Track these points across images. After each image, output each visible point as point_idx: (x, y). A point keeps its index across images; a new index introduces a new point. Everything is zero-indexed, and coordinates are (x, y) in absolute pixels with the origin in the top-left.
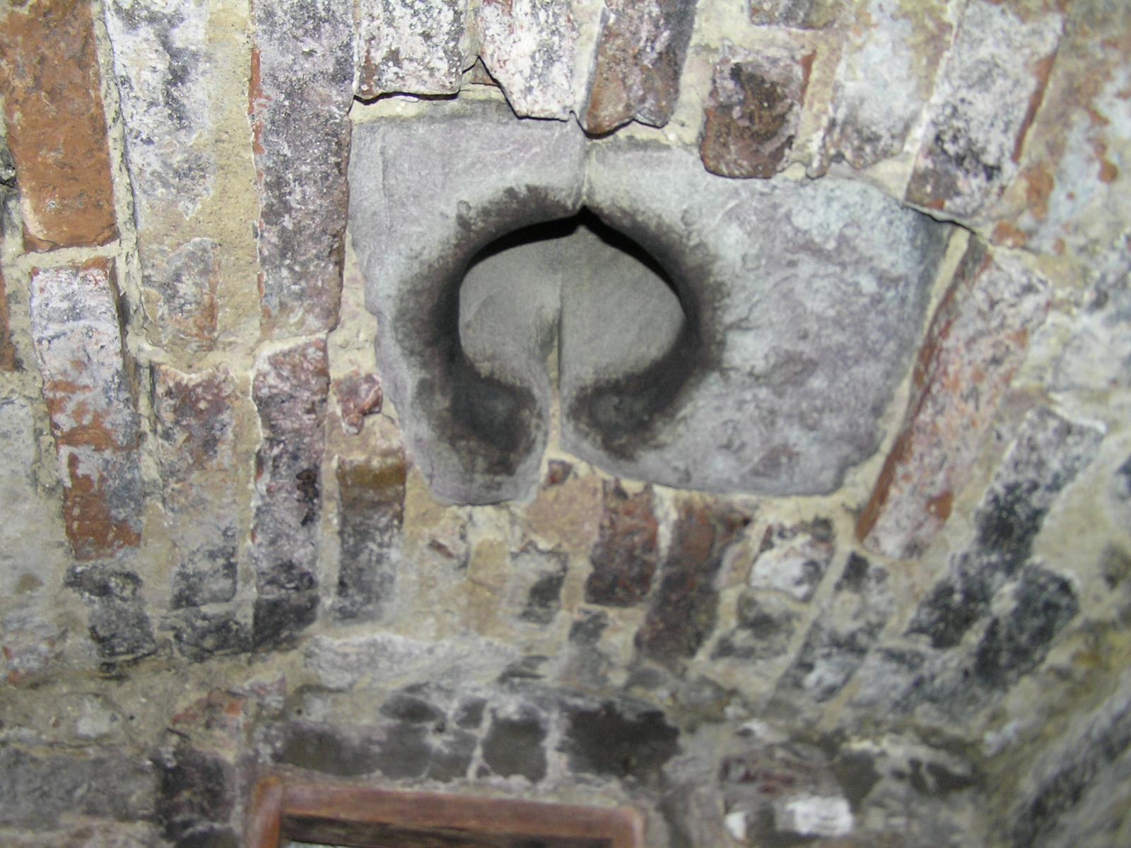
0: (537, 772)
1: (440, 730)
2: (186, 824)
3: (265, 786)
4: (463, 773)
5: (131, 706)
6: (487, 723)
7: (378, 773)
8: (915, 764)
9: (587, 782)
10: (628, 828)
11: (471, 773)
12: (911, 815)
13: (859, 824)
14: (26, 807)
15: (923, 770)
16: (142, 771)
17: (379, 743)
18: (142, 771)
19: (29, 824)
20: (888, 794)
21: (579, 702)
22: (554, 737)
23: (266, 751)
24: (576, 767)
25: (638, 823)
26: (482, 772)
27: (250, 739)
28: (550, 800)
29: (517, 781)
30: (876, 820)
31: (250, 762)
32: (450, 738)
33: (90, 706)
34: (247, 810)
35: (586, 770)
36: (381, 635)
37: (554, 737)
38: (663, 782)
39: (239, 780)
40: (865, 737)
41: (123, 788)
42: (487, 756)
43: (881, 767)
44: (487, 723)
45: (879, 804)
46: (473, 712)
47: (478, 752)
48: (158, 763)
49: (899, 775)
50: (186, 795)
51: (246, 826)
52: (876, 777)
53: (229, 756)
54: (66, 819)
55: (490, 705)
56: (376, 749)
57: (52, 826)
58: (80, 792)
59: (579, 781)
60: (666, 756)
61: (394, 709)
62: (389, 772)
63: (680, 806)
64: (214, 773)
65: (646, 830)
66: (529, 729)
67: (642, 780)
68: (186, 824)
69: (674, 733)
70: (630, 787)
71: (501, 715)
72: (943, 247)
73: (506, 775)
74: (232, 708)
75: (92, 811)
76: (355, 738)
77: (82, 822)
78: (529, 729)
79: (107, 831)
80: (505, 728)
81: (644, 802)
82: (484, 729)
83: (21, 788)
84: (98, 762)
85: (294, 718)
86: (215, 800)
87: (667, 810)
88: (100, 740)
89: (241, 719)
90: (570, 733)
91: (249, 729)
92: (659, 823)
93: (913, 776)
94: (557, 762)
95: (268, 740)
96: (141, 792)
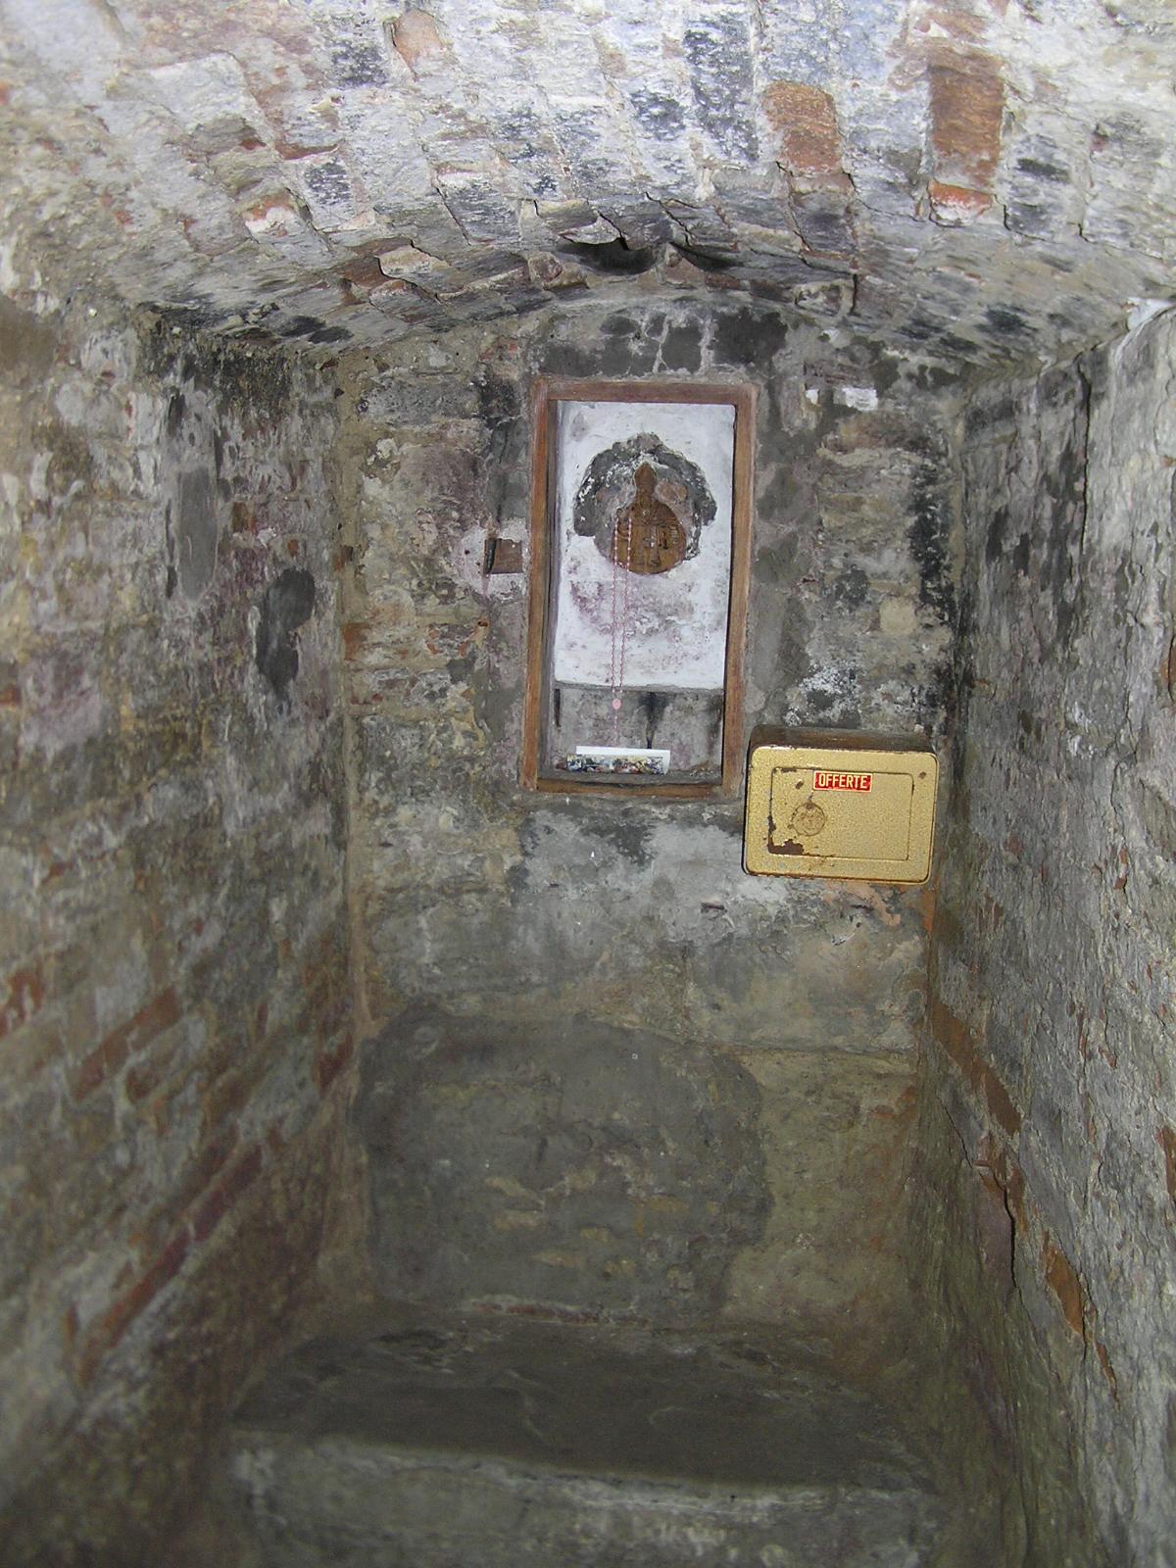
0: (694, 366)
1: (638, 337)
2: (498, 419)
3: (538, 385)
4: (651, 369)
5: (456, 344)
6: (665, 333)
7: (675, 1512)
8: (923, 368)
9: (725, 369)
10: (748, 397)
11: (655, 368)
12: (911, 404)
13: (881, 405)
14: (413, 413)
15: (927, 373)
16: (468, 389)
17: (600, 352)
18: (468, 389)
19: (416, 422)
20: (900, 390)
21: (725, 310)
22: (707, 337)
23: (535, 366)
24: (719, 359)
25: (754, 395)
26: (661, 367)
27: (526, 361)
28: (703, 380)
29: (683, 371)
30: (890, 405)
31: (527, 377)
32: (642, 344)
33: (433, 350)
34: (529, 403)
35: (725, 361)
36: (593, 302)
37: (707, 337)
38: (771, 369)
39: (523, 390)
40: (896, 348)
41: (460, 400)
42: (664, 356)
43: (901, 370)
44: (665, 333)
45: (893, 397)
46: (657, 322)
47: (660, 353)
48: (477, 384)
49: (910, 376)
50: (495, 402)
51: (529, 412)
52: (896, 377)
53: (515, 376)
54: (434, 418)
55: (667, 318)
56: (599, 356)
57: (429, 422)
58: (439, 402)
59: (720, 369)
60: (775, 349)
61: (605, 328)
62: (608, 373)
63: (777, 388)
64: (508, 389)
65: (758, 399)
66: (692, 333)
67: (759, 365)
68: (498, 419)
69: (785, 328)
70: (750, 371)
71: (674, 325)
72: (747, 548)
73: (676, 369)
74: (513, 347)
75: (447, 414)
76: (586, 350)
77: (444, 420)
78: (692, 333)
79: (457, 425)
80: (677, 334)
81: (758, 381)
82: (662, 338)
83: (407, 402)
84: (445, 385)
85: (550, 340)
86: (511, 405)
87: (771, 389)
88: (442, 371)
89: (519, 352)
90: (716, 334)
91: (524, 355)
92: (765, 397)
93: (919, 379)
94: (707, 356)
95: (536, 359)
96: (471, 402)
